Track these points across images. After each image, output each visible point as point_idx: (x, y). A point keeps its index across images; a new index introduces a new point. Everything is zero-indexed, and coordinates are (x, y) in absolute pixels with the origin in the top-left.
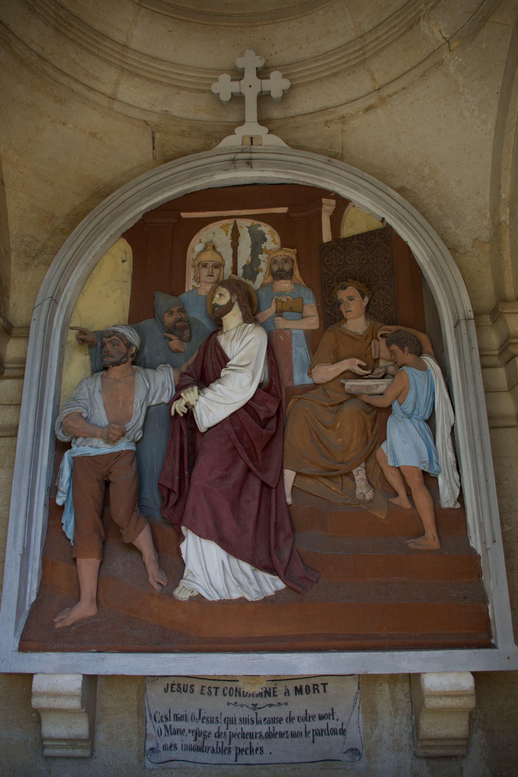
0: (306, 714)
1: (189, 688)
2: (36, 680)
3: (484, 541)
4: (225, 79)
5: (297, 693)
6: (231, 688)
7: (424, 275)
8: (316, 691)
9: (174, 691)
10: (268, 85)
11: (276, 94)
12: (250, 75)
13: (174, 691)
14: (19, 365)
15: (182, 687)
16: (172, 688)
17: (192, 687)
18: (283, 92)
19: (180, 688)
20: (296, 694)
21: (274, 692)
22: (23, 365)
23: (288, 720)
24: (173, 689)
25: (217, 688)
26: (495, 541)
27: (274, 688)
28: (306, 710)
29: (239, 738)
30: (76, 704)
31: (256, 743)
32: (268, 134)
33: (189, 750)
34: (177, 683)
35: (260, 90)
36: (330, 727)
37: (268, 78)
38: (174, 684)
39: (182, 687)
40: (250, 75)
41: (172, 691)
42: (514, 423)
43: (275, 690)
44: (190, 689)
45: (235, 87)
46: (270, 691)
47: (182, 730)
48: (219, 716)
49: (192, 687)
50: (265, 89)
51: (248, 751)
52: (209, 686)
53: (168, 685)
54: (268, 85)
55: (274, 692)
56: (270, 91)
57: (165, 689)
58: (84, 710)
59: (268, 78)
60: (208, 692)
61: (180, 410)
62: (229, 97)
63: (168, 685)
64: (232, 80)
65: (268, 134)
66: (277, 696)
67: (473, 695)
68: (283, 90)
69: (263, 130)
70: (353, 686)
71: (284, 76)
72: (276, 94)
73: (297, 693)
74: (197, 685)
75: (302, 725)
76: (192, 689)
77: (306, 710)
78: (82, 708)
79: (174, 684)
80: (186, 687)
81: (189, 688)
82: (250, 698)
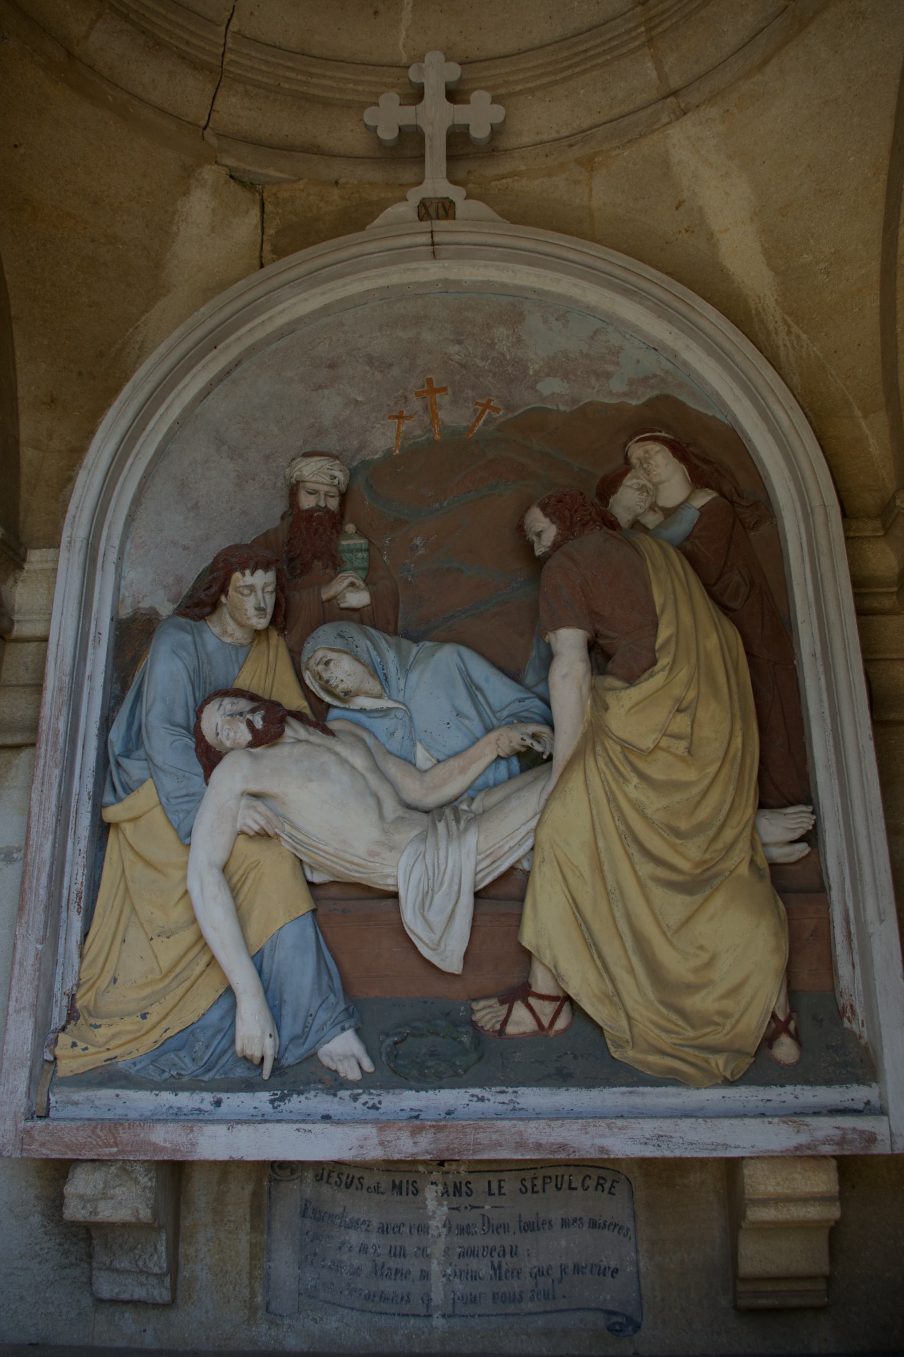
4: (390, 101)
7: (201, 810)
8: (600, 1187)
16: (329, 1176)
18: (492, 129)
21: (500, 1187)
24: (503, 1191)
28: (520, 1215)
29: (467, 1278)
32: (465, 199)
35: (450, 123)
37: (467, 102)
39: (344, 1178)
44: (466, 1189)
45: (407, 115)
47: (404, 1272)
52: (468, 1180)
55: (500, 1187)
56: (468, 126)
59: (467, 102)
60: (336, 1182)
68: (492, 125)
69: (456, 194)
71: (495, 100)
72: (480, 132)
76: (469, 1189)
77: (520, 1215)
79: (333, 1172)
81: (464, 1189)
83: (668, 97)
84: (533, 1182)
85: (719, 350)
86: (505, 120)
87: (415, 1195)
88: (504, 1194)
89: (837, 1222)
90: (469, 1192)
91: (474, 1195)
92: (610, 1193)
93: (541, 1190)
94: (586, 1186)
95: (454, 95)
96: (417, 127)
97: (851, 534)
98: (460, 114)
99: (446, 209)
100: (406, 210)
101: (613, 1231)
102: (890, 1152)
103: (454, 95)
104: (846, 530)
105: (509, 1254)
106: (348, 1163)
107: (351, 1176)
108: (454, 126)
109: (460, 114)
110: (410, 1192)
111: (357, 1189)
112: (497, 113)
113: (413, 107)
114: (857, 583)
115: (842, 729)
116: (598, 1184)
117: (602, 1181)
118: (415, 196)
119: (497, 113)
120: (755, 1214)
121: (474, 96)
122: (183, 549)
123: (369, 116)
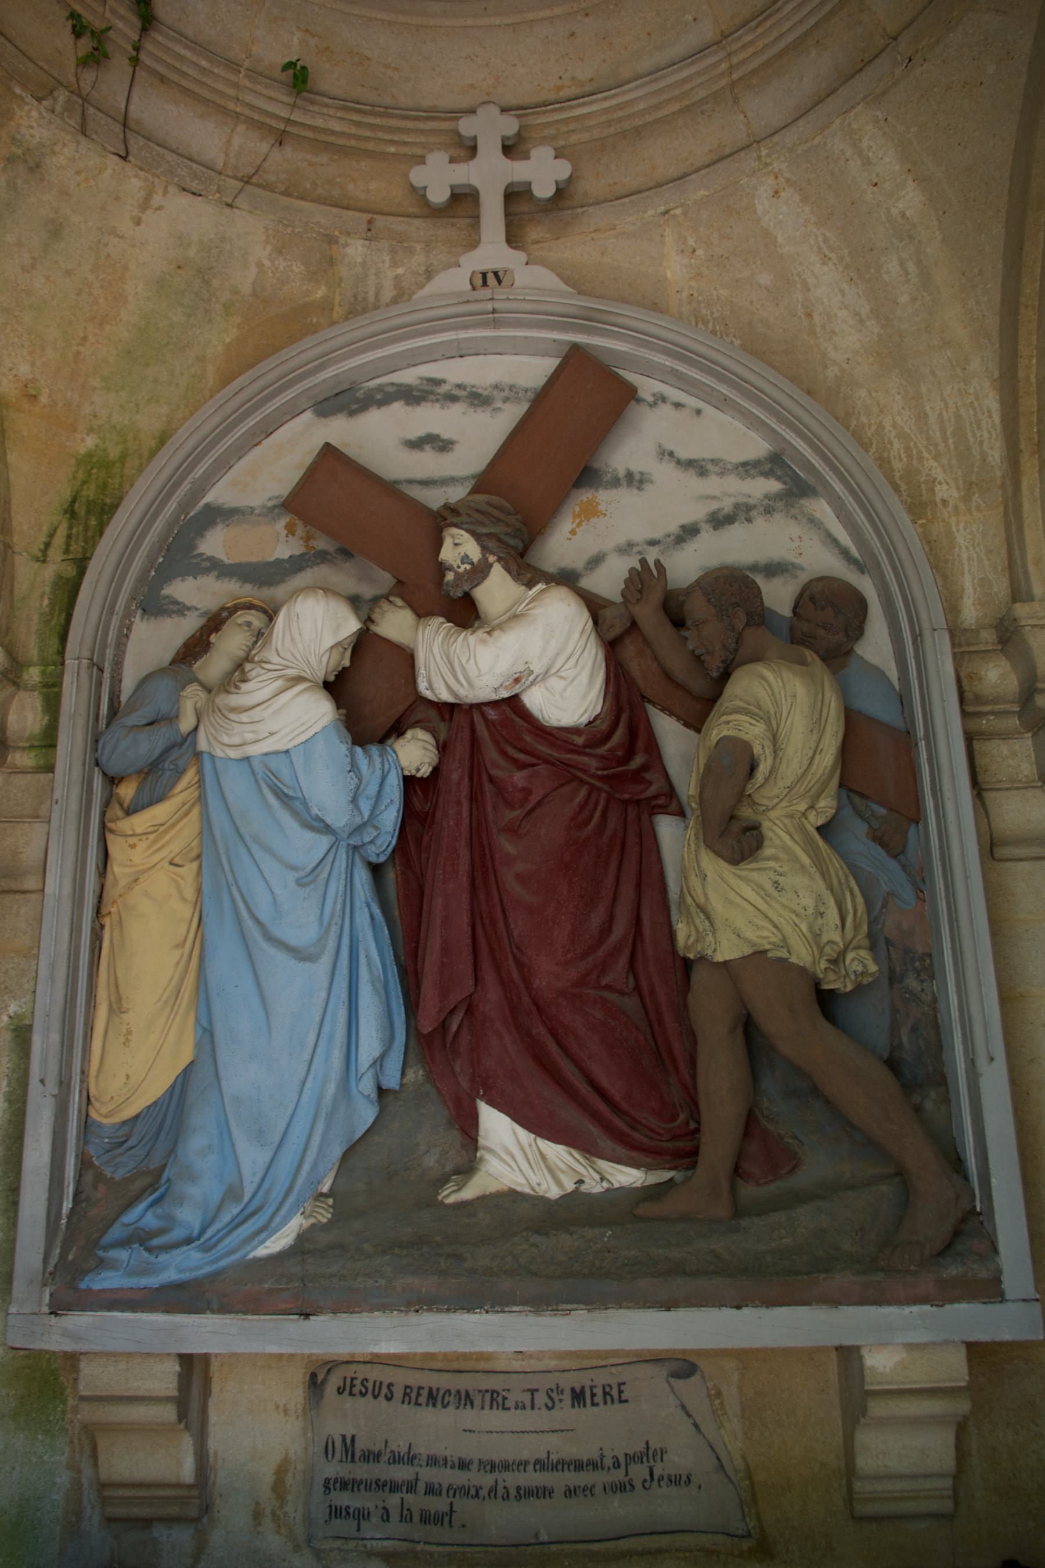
0: (648, 1448)
1: (384, 1390)
2: (87, 1369)
3: (971, 1057)
4: (438, 159)
5: (576, 1404)
15: (370, 1386)
17: (365, 1382)
19: (366, 1389)
20: (573, 1406)
21: (620, 1392)
24: (624, 1397)
26: (992, 1059)
27: (619, 1385)
33: (552, 1470)
34: (360, 1376)
37: (528, 158)
38: (356, 1378)
39: (370, 1386)
40: (466, 174)
41: (351, 1394)
43: (622, 1387)
46: (466, 1400)
49: (365, 1382)
53: (345, 1378)
55: (620, 1392)
56: (530, 184)
57: (339, 1388)
59: (528, 158)
61: (277, 646)
63: (345, 1378)
70: (834, 1355)
72: (544, 191)
73: (576, 1404)
79: (595, 1387)
81: (384, 1390)
82: (484, 1412)
84: (619, 1388)
85: (876, 519)
88: (626, 1401)
90: (389, 1396)
92: (621, 1401)
93: (601, 1402)
94: (446, 1402)
95: (511, 149)
96: (470, 186)
98: (519, 171)
101: (563, 1471)
102: (562, 1193)
103: (511, 149)
105: (414, 1514)
107: (378, 1384)
108: (510, 185)
109: (519, 171)
112: (563, 170)
115: (930, 704)
116: (605, 1394)
117: (408, 1391)
121: (534, 153)
123: (418, 176)
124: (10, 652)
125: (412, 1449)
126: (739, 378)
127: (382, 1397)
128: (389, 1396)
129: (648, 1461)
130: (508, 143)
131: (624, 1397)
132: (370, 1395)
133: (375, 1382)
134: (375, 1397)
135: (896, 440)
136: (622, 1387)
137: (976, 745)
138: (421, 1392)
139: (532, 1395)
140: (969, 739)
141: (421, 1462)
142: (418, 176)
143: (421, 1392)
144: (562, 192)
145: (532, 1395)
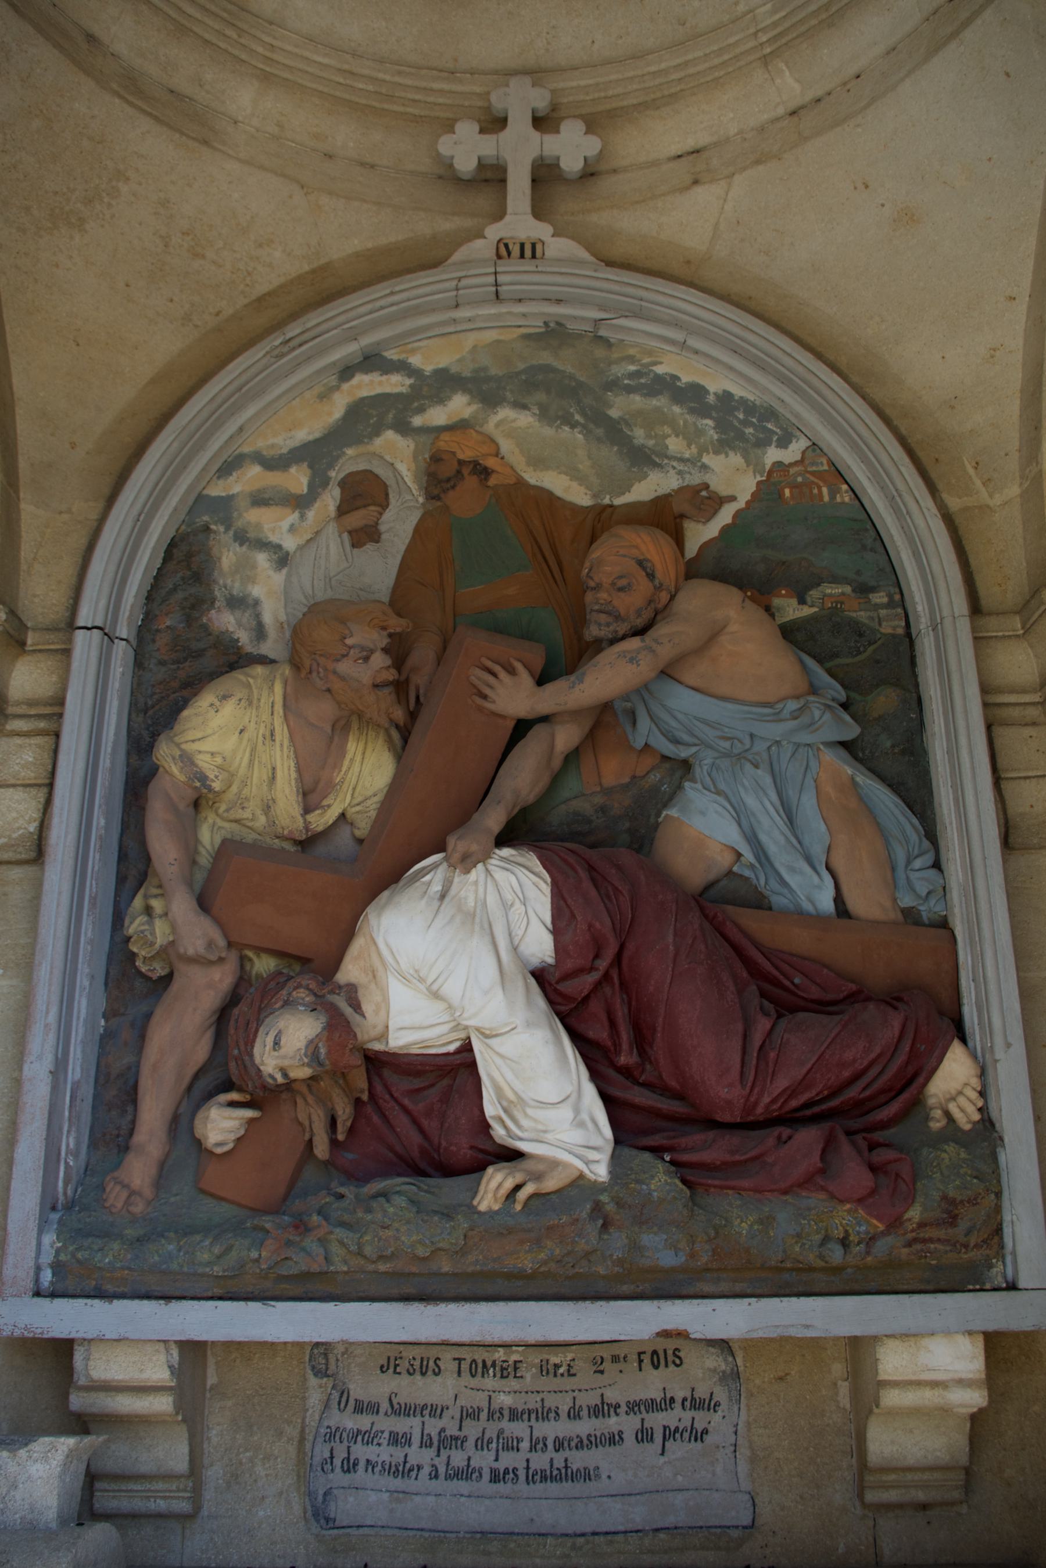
4: (467, 129)
6: (474, 1361)
9: (399, 1373)
10: (553, 145)
11: (572, 164)
12: (519, 123)
13: (399, 1373)
14: (48, 710)
21: (516, 1369)
22: (56, 709)
23: (688, 1404)
24: (398, 1370)
25: (459, 1360)
26: (1008, 1045)
30: (163, 1404)
31: (579, 1459)
32: (553, 236)
36: (533, 1466)
37: (558, 132)
38: (644, 1353)
40: (519, 123)
42: (1033, 713)
45: (487, 146)
48: (451, 1403)
50: (546, 152)
51: (686, 1435)
53: (389, 1358)
54: (553, 145)
56: (558, 158)
57: (382, 1367)
58: (180, 1418)
59: (558, 132)
62: (473, 164)
63: (389, 1358)
64: (482, 131)
65: (553, 236)
66: (574, 1375)
67: (307, 829)
68: (585, 159)
69: (542, 231)
72: (572, 164)
74: (447, 1358)
75: (688, 1415)
78: (177, 1413)
79: (644, 1353)
80: (425, 1363)
83: (332, 1453)
86: (601, 151)
87: (677, 1366)
89: (981, 1411)
90: (437, 1370)
91: (684, 1366)
95: (542, 122)
97: (977, 635)
99: (530, 251)
100: (482, 248)
103: (542, 122)
104: (974, 629)
106: (1003, 830)
110: (670, 1363)
111: (414, 1359)
112: (592, 145)
113: (494, 137)
114: (985, 689)
118: (494, 232)
119: (592, 145)
120: (891, 1398)
122: (154, 234)
123: (445, 146)
124: (12, 613)
125: (408, 1459)
126: (766, 354)
127: (430, 1373)
128: (437, 1370)
129: (529, 1420)
130: (540, 114)
131: (572, 1371)
132: (418, 1373)
133: (422, 1359)
134: (423, 1374)
135: (814, 594)
136: (518, 1365)
137: (997, 731)
138: (642, 1356)
139: (460, 1364)
140: (989, 728)
141: (381, 1441)
142: (445, 146)
143: (642, 1356)
144: (589, 173)
145: (460, 1364)
